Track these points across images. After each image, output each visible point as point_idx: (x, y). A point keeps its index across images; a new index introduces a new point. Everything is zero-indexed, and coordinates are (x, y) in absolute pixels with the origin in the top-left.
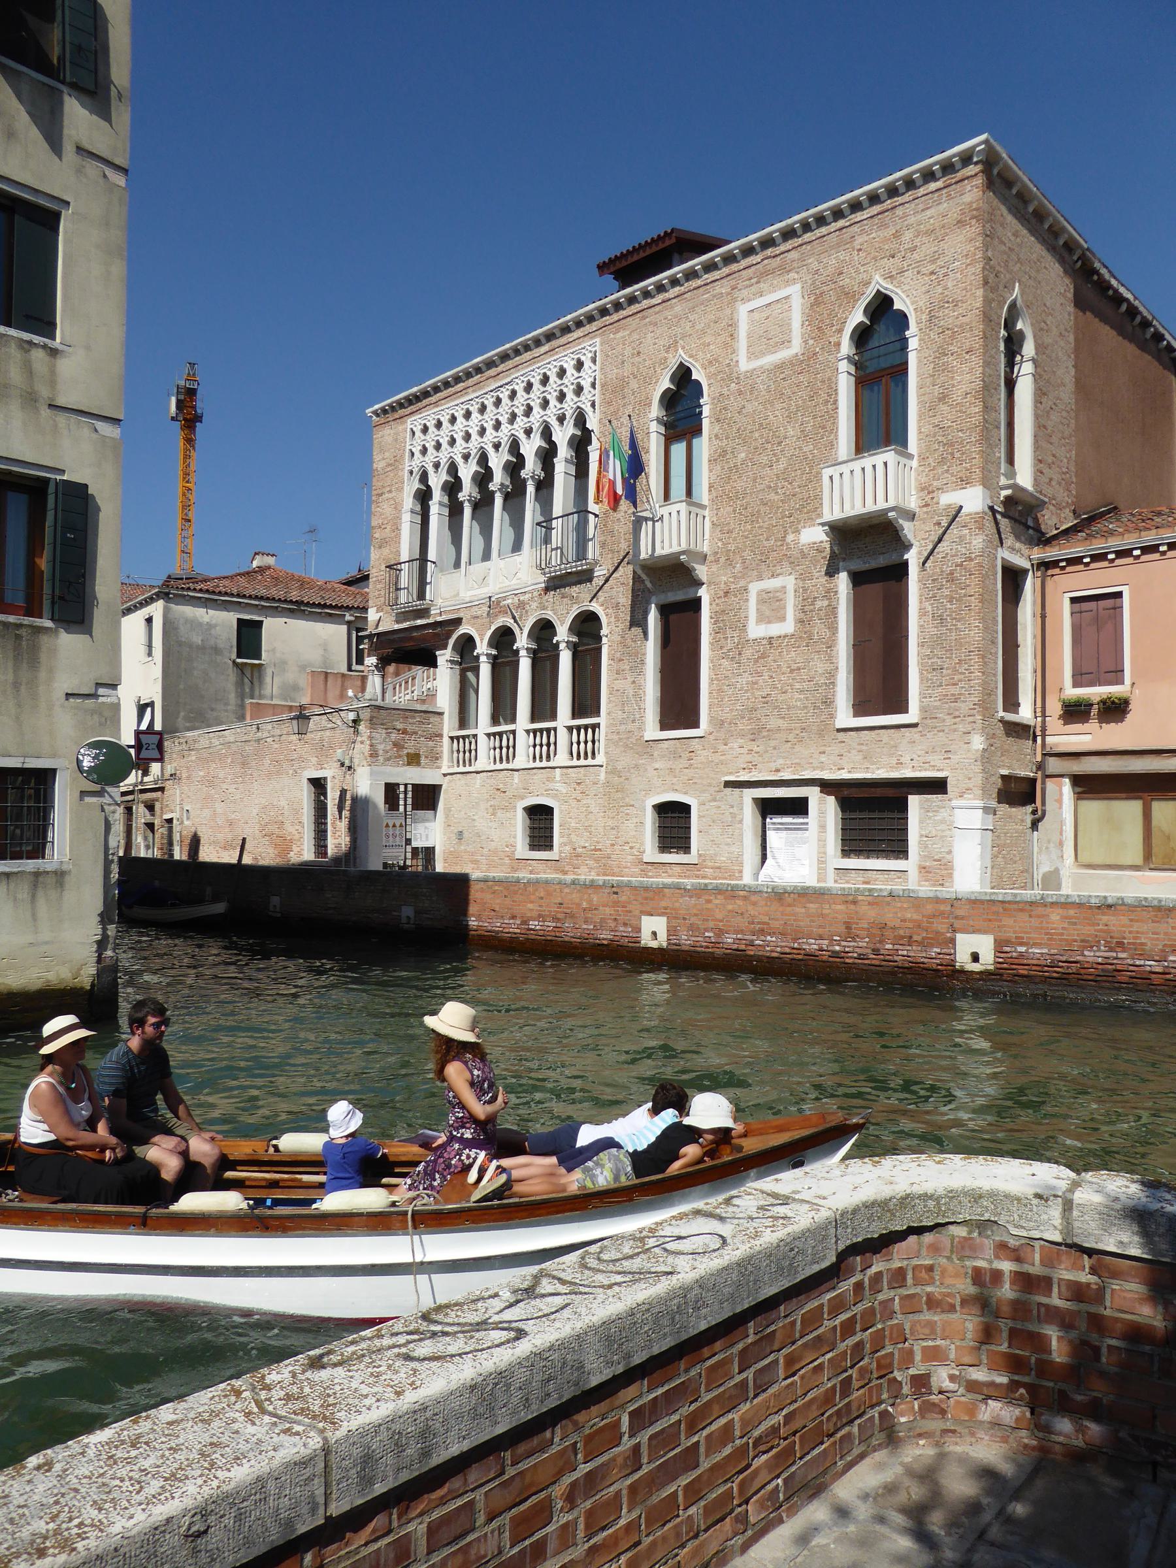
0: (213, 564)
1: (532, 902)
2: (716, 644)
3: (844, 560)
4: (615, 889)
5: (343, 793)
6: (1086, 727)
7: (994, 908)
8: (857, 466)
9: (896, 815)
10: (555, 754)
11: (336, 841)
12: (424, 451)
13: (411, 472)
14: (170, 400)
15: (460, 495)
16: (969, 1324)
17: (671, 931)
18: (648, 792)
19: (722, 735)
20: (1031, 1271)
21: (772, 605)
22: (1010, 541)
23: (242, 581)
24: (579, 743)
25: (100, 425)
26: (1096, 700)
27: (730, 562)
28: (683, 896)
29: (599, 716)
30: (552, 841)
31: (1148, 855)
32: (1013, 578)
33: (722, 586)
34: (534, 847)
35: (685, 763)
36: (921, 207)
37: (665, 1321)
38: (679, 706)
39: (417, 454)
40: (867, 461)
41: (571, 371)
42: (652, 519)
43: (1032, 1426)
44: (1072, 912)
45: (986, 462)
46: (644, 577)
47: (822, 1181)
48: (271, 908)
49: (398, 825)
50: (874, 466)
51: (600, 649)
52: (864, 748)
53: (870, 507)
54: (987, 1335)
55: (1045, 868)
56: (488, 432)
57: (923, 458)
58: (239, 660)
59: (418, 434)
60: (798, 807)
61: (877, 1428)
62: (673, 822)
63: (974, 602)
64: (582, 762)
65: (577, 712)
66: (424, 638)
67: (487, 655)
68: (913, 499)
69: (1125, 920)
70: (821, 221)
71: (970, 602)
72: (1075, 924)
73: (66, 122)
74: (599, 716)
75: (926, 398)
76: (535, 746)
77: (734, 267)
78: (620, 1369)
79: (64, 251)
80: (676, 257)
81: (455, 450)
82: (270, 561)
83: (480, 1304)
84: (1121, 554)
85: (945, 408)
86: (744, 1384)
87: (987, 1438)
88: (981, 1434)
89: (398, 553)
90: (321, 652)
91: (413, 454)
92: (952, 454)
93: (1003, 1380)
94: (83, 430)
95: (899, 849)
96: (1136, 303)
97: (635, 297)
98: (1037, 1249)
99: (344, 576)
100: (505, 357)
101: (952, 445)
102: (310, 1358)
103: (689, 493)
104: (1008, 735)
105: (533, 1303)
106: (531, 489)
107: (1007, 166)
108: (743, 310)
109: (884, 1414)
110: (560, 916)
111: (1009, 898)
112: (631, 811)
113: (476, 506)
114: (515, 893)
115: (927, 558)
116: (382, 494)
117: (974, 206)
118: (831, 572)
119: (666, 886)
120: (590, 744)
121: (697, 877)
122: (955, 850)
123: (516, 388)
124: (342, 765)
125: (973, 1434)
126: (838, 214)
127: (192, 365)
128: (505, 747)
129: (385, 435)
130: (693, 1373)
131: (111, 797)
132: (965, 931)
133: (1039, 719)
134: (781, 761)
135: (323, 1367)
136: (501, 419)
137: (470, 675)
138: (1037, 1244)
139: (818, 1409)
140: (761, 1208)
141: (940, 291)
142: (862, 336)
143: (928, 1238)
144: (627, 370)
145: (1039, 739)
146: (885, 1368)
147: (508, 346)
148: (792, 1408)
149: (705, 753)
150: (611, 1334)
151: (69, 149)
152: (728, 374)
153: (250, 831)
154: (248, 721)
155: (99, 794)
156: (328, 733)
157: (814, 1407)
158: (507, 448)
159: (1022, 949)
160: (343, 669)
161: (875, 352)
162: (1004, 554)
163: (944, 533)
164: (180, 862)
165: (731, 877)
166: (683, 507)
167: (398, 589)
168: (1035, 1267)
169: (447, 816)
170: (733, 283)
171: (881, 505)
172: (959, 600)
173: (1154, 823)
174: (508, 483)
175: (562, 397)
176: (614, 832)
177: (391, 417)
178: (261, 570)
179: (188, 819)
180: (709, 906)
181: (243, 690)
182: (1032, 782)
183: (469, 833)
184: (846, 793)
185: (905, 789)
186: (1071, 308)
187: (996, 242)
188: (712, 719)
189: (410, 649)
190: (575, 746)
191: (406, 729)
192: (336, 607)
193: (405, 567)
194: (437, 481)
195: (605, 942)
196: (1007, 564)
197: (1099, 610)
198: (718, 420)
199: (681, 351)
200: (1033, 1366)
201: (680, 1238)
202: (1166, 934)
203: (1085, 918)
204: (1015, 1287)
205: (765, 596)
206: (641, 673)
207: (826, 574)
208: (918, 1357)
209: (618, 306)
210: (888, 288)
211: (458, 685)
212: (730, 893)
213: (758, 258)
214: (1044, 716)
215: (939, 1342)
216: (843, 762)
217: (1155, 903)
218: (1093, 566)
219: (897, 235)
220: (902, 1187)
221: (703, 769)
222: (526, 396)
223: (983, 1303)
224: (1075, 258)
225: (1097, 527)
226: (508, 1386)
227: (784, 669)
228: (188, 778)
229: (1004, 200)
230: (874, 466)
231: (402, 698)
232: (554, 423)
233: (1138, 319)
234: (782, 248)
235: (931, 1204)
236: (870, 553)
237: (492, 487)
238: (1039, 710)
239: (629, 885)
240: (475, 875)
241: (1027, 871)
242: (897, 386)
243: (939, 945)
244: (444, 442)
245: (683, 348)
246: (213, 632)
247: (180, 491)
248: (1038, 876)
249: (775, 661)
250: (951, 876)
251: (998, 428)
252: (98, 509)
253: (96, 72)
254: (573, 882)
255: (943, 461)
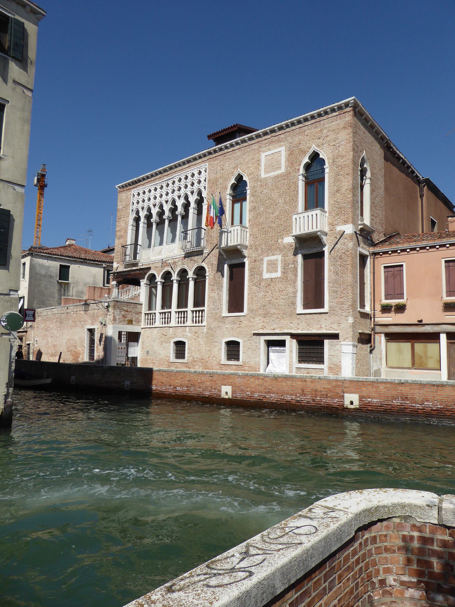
0: (49, 243)
1: (178, 380)
2: (250, 280)
3: (300, 250)
4: (211, 375)
5: (102, 335)
6: (390, 315)
7: (359, 384)
8: (306, 215)
9: (319, 347)
10: (187, 321)
11: (98, 354)
12: (138, 202)
13: (133, 210)
14: (34, 178)
15: (152, 220)
16: (401, 558)
17: (234, 392)
18: (223, 337)
19: (252, 315)
20: (425, 536)
21: (272, 266)
22: (362, 244)
23: (62, 250)
24: (196, 317)
25: (16, 187)
26: (394, 304)
27: (256, 249)
28: (238, 378)
29: (204, 307)
30: (184, 355)
31: (413, 364)
32: (363, 258)
33: (253, 258)
34: (177, 357)
35: (238, 326)
36: (330, 121)
37: (301, 565)
38: (236, 303)
39: (135, 204)
40: (310, 213)
41: (196, 175)
42: (227, 232)
43: (426, 599)
44: (388, 385)
45: (354, 215)
46: (223, 254)
47: (343, 501)
48: (71, 381)
49: (123, 348)
50: (312, 215)
51: (205, 280)
52: (307, 321)
53: (311, 230)
54: (409, 561)
55: (375, 368)
56: (163, 196)
57: (330, 213)
58: (60, 281)
59: (136, 196)
60: (282, 344)
61: (367, 602)
62: (233, 349)
63: (349, 267)
64: (197, 324)
65: (196, 305)
66: (135, 275)
67: (161, 282)
68: (327, 228)
69: (408, 389)
70: (293, 124)
71: (348, 267)
72: (389, 390)
73: (10, 71)
74: (204, 307)
75: (331, 191)
76: (178, 318)
77: (260, 139)
78: (287, 586)
79: (6, 120)
80: (237, 134)
81: (150, 203)
82: (73, 242)
83: (228, 560)
84: (403, 251)
85: (338, 195)
86: (325, 588)
87: (408, 604)
88: (406, 602)
89: (126, 241)
90: (93, 279)
91: (133, 203)
92: (341, 212)
93: (414, 580)
94: (10, 189)
95: (321, 361)
96: (405, 159)
97: (222, 148)
98: (428, 527)
99: (102, 249)
100: (171, 168)
101: (341, 208)
102: (166, 587)
103: (241, 222)
104: (361, 317)
105: (250, 559)
106: (179, 218)
107: (361, 108)
108: (263, 155)
109: (370, 596)
110: (189, 385)
111: (364, 380)
112: (216, 344)
113: (158, 224)
114: (171, 376)
115: (332, 250)
116: (121, 218)
117: (350, 122)
118: (295, 254)
119: (232, 374)
120: (200, 318)
121: (242, 370)
122: (342, 361)
123: (175, 180)
124: (102, 323)
125: (403, 603)
126: (299, 122)
127: (44, 165)
128: (167, 318)
129: (123, 196)
130: (309, 585)
131: (13, 335)
132: (348, 392)
133: (373, 311)
134: (275, 326)
135: (174, 591)
136: (169, 191)
137: (153, 290)
138: (428, 525)
139: (349, 596)
140: (324, 513)
141: (337, 152)
142: (307, 167)
143: (385, 523)
144: (218, 175)
145: (372, 319)
146: (369, 577)
147: (172, 164)
148: (340, 596)
149: (246, 322)
150: (284, 571)
151: (10, 81)
152: (257, 179)
153: (63, 349)
154: (62, 305)
155: (9, 334)
156: (96, 311)
157: (347, 596)
158: (171, 203)
159: (370, 400)
160: (101, 285)
161: (312, 173)
162: (360, 249)
163: (338, 241)
164: (32, 361)
165: (255, 371)
166: (239, 228)
167: (125, 255)
168: (427, 534)
169: (143, 345)
170: (259, 145)
171: (315, 230)
172: (344, 266)
173: (416, 351)
174: (170, 216)
175: (193, 184)
176: (210, 352)
177: (125, 189)
178: (70, 246)
179: (36, 344)
180: (249, 382)
181: (61, 293)
182: (371, 335)
183: (152, 351)
184: (300, 338)
185: (323, 338)
186: (383, 160)
187: (357, 135)
188: (249, 309)
189: (130, 279)
190: (195, 318)
191: (127, 310)
192: (99, 261)
193: (129, 247)
194: (142, 214)
195: (207, 396)
196: (361, 253)
197: (394, 272)
198: (253, 196)
199: (239, 169)
200: (427, 574)
201: (298, 528)
202: (423, 394)
203: (393, 388)
204: (419, 542)
205: (270, 263)
206: (221, 290)
207: (293, 255)
208: (381, 572)
209: (215, 151)
210: (318, 150)
211: (149, 293)
212: (257, 377)
213: (269, 136)
214: (374, 310)
215: (389, 566)
216: (299, 327)
217: (419, 382)
218: (392, 255)
219: (321, 131)
220: (375, 503)
221: (245, 327)
222: (179, 183)
223: (406, 549)
224: (384, 142)
225: (392, 240)
226: (250, 596)
227: (277, 290)
228: (37, 327)
229: (360, 120)
230: (312, 215)
231: (125, 297)
232: (189, 194)
233: (406, 165)
234: (278, 133)
235: (386, 509)
236: (310, 248)
237: (164, 217)
238: (372, 308)
239: (217, 373)
240: (155, 369)
241: (368, 369)
242: (320, 185)
243: (338, 398)
244: (146, 199)
245: (240, 168)
246: (50, 269)
247: (37, 213)
248: (372, 371)
249: (273, 287)
250: (340, 371)
251: (358, 203)
252: (14, 220)
253: (22, 53)
254: (195, 372)
255: (338, 214)
